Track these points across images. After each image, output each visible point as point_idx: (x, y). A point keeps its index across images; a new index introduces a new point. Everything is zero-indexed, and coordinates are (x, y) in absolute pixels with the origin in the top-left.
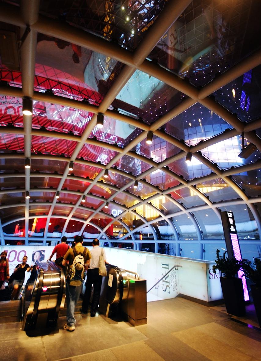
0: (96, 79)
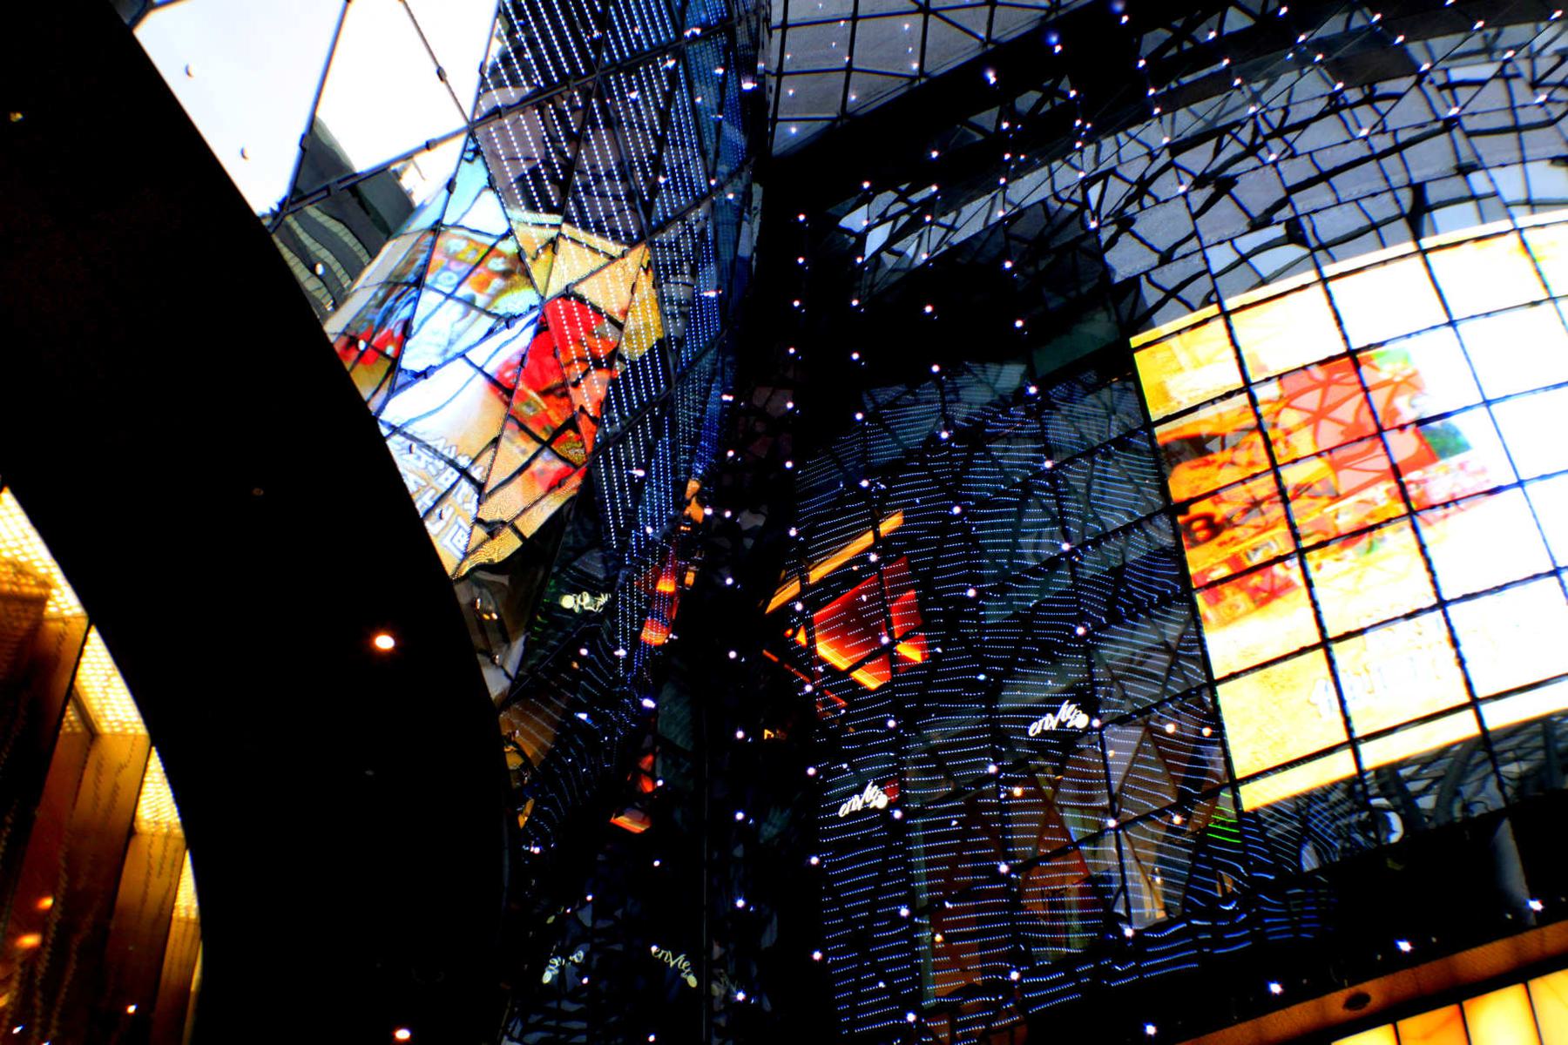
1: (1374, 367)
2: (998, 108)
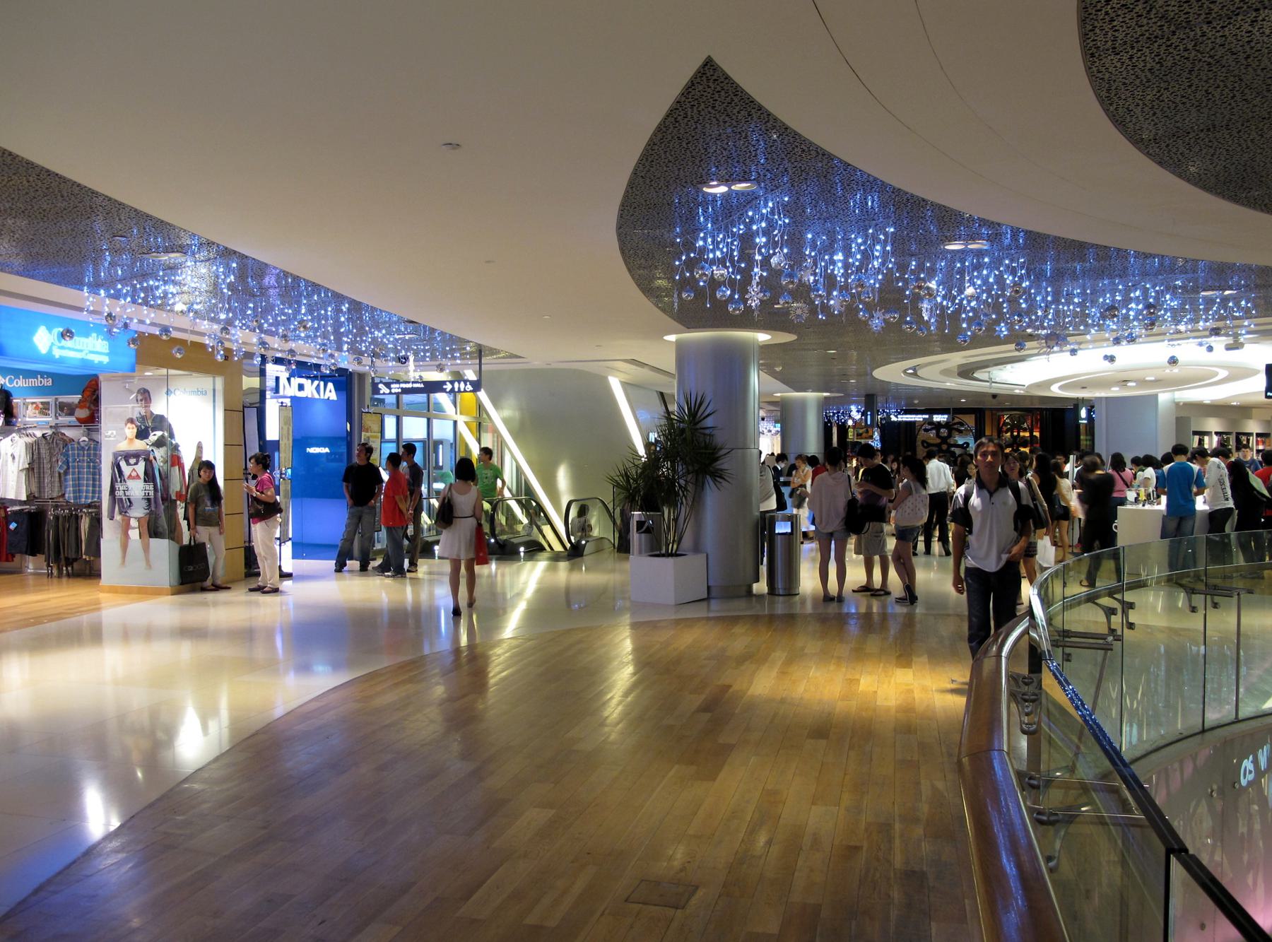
0: (648, 439)
1: (612, 479)
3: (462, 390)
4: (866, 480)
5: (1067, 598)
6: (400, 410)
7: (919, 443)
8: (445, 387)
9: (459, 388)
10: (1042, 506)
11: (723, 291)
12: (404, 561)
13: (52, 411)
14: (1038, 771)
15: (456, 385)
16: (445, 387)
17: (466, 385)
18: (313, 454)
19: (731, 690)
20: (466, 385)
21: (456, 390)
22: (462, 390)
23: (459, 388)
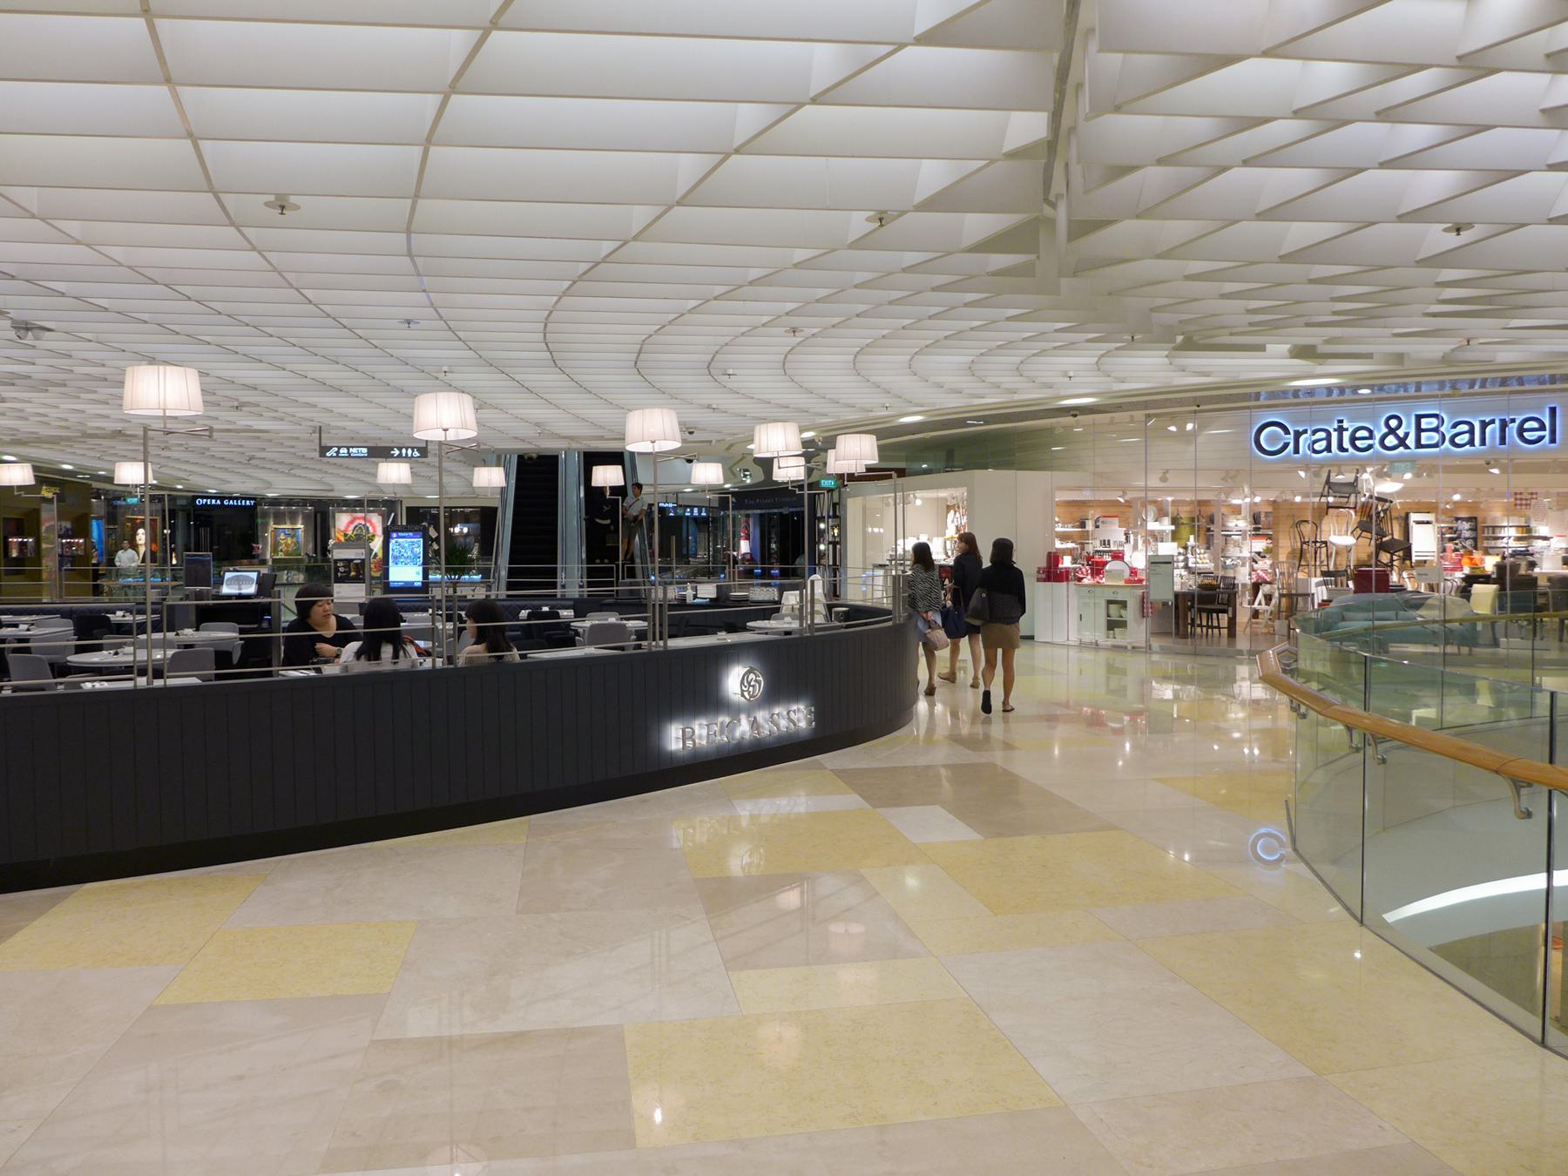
2: (1384, 916)
3: (410, 455)
4: (482, 555)
5: (1450, 621)
6: (1558, 766)
7: (1317, 694)
8: (392, 452)
9: (407, 454)
10: (807, 608)
11: (675, 512)
12: (797, 590)
13: (106, 589)
14: (1097, 111)
15: (404, 451)
16: (392, 452)
17: (413, 451)
18: (240, 658)
19: (1071, 701)
20: (413, 451)
21: (404, 455)
22: (410, 455)
23: (407, 454)
